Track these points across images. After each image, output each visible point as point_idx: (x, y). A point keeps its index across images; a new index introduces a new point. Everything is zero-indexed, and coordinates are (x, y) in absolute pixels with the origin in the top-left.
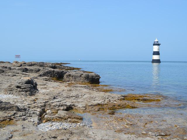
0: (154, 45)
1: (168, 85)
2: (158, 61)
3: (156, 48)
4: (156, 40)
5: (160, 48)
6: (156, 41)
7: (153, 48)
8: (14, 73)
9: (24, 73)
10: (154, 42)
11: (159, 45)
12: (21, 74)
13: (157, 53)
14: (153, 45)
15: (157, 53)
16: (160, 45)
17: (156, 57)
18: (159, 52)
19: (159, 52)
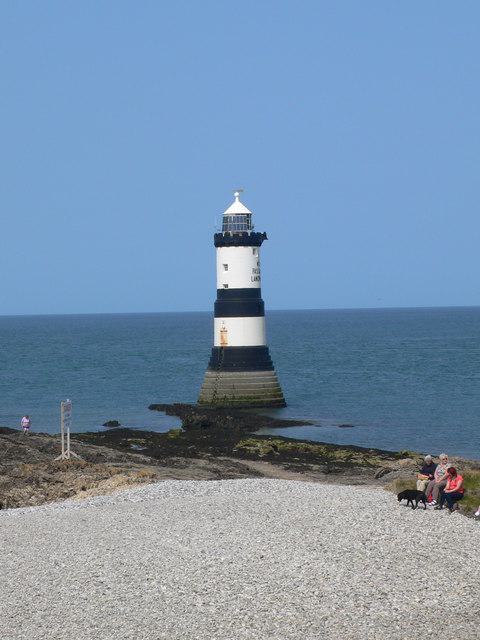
0: (222, 241)
4: (237, 208)
10: (226, 219)
11: (254, 240)
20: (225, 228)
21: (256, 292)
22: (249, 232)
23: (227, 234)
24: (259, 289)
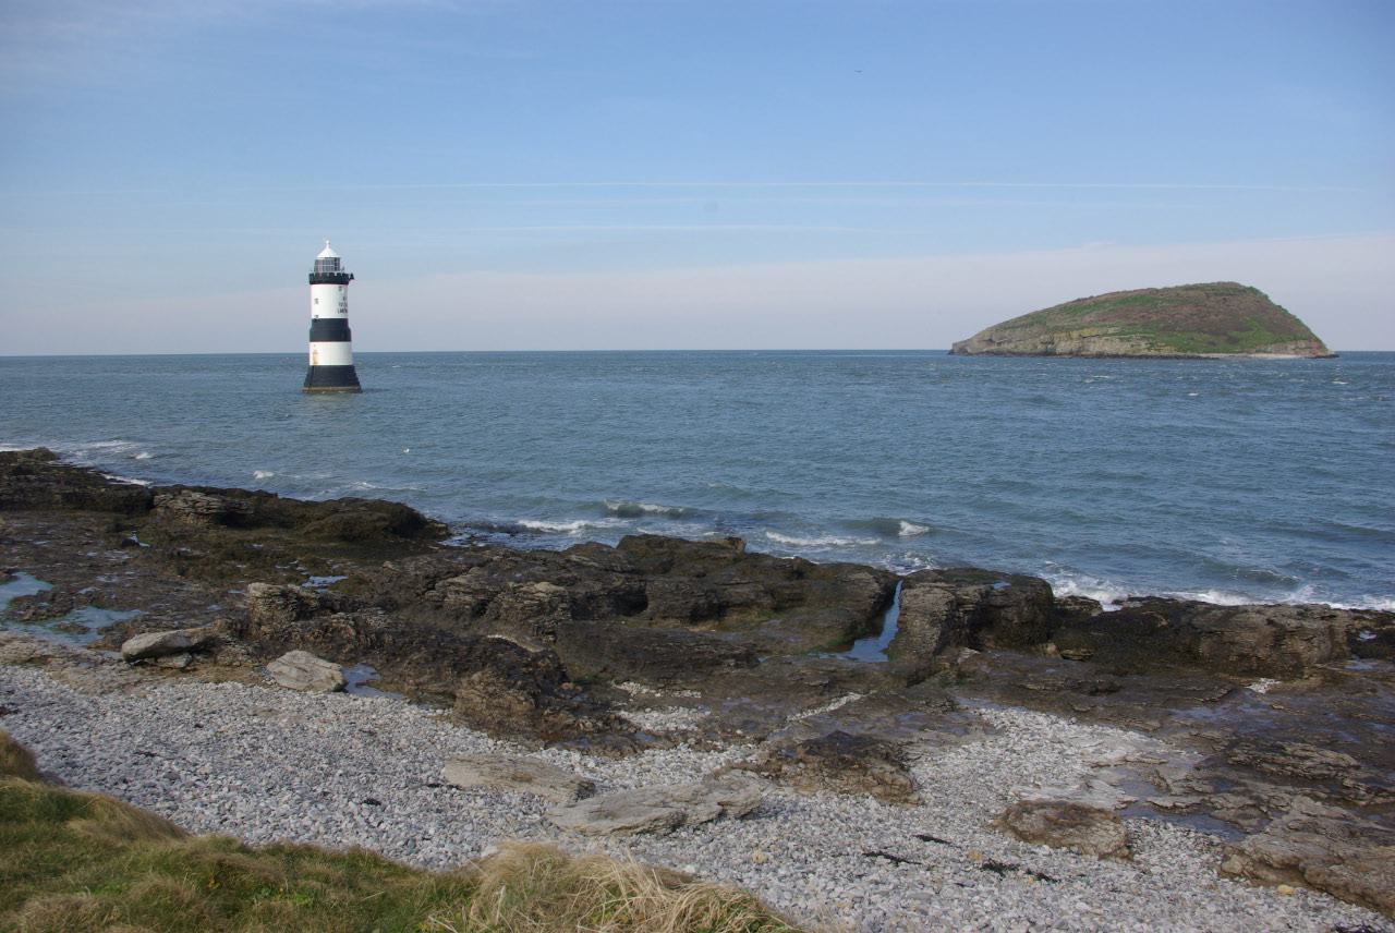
0: (315, 279)
1: (1111, 470)
2: (343, 377)
3: (324, 302)
4: (327, 253)
5: (349, 301)
6: (326, 261)
7: (307, 302)
8: (960, 419)
9: (313, 389)
10: (317, 262)
11: (342, 280)
12: (1322, 724)
13: (335, 330)
14: (307, 280)
15: (335, 330)
16: (351, 282)
17: (326, 354)
18: (343, 322)
19: (343, 322)
20: (316, 269)
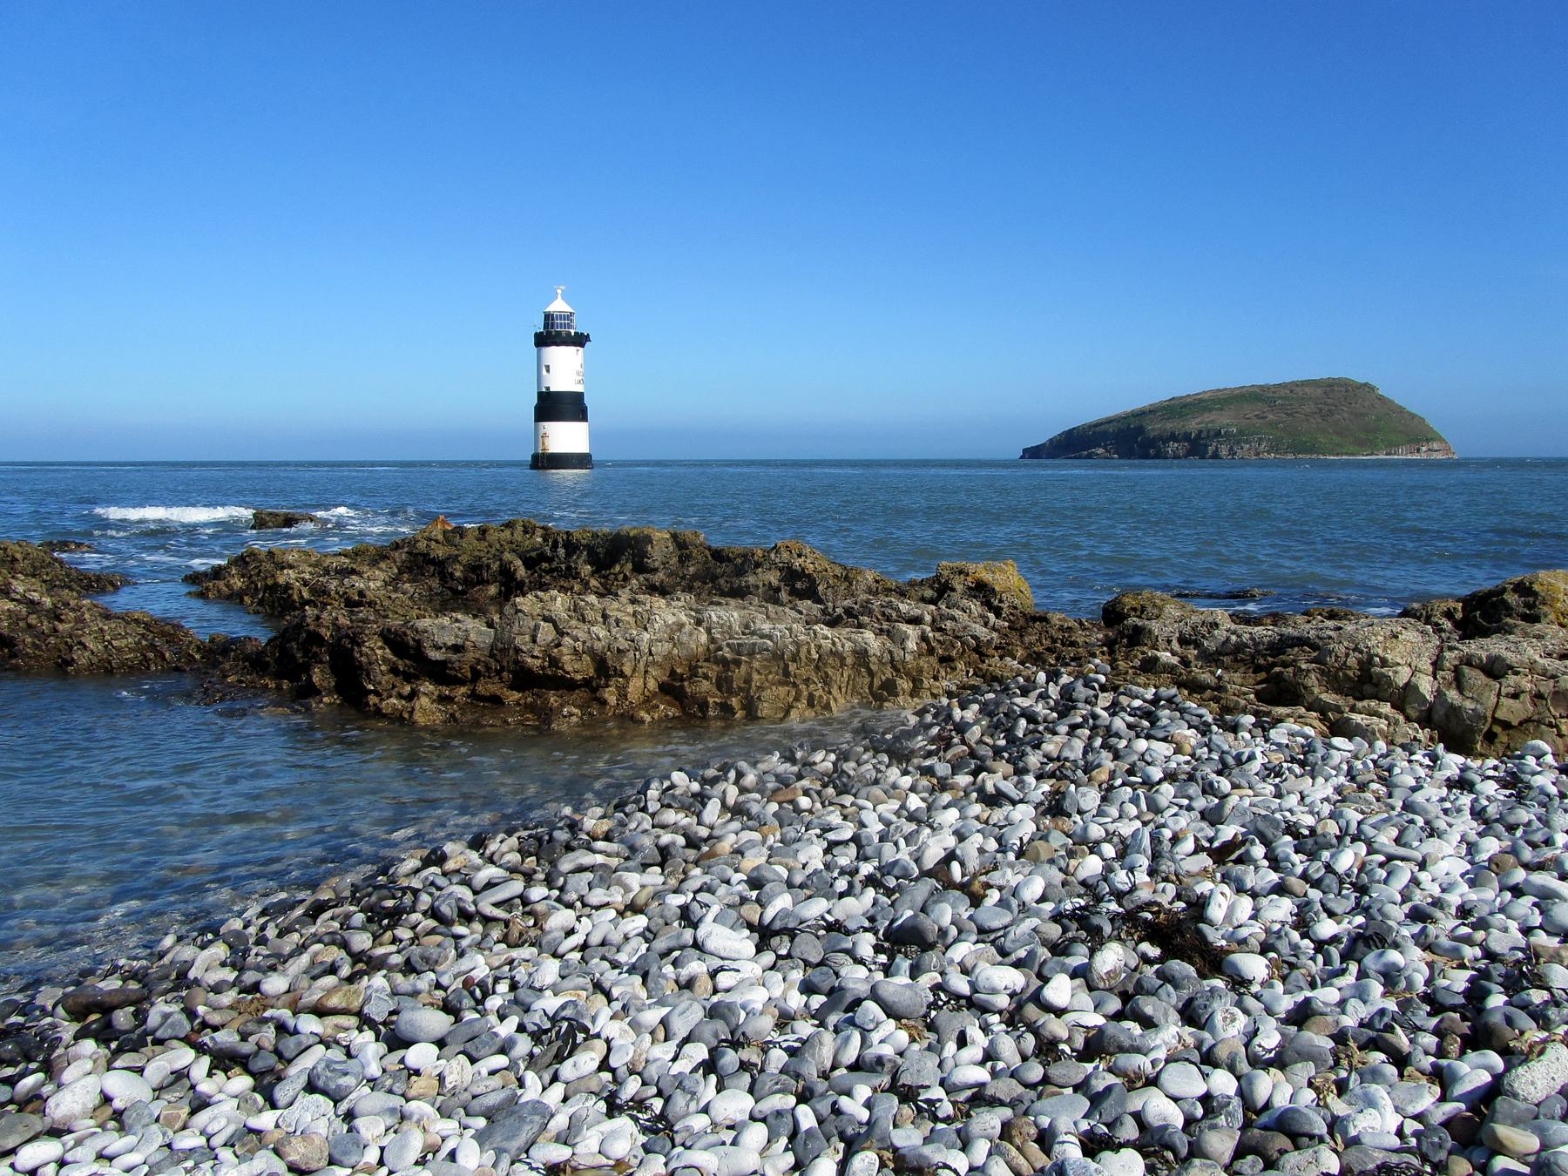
0: (543, 340)
4: (559, 306)
11: (580, 340)
20: (546, 326)
21: (579, 397)
22: (573, 332)
23: (549, 333)
24: (581, 395)
